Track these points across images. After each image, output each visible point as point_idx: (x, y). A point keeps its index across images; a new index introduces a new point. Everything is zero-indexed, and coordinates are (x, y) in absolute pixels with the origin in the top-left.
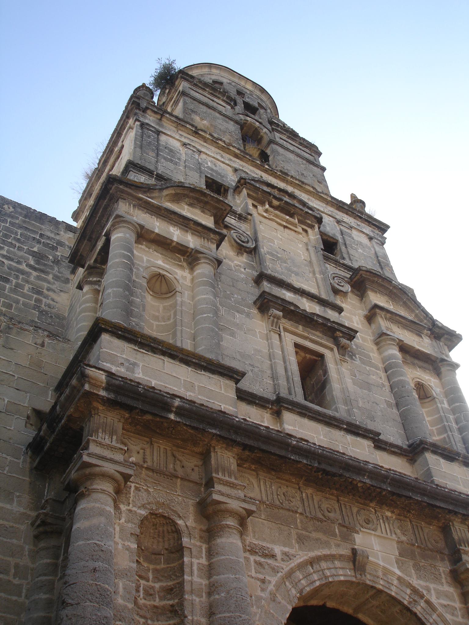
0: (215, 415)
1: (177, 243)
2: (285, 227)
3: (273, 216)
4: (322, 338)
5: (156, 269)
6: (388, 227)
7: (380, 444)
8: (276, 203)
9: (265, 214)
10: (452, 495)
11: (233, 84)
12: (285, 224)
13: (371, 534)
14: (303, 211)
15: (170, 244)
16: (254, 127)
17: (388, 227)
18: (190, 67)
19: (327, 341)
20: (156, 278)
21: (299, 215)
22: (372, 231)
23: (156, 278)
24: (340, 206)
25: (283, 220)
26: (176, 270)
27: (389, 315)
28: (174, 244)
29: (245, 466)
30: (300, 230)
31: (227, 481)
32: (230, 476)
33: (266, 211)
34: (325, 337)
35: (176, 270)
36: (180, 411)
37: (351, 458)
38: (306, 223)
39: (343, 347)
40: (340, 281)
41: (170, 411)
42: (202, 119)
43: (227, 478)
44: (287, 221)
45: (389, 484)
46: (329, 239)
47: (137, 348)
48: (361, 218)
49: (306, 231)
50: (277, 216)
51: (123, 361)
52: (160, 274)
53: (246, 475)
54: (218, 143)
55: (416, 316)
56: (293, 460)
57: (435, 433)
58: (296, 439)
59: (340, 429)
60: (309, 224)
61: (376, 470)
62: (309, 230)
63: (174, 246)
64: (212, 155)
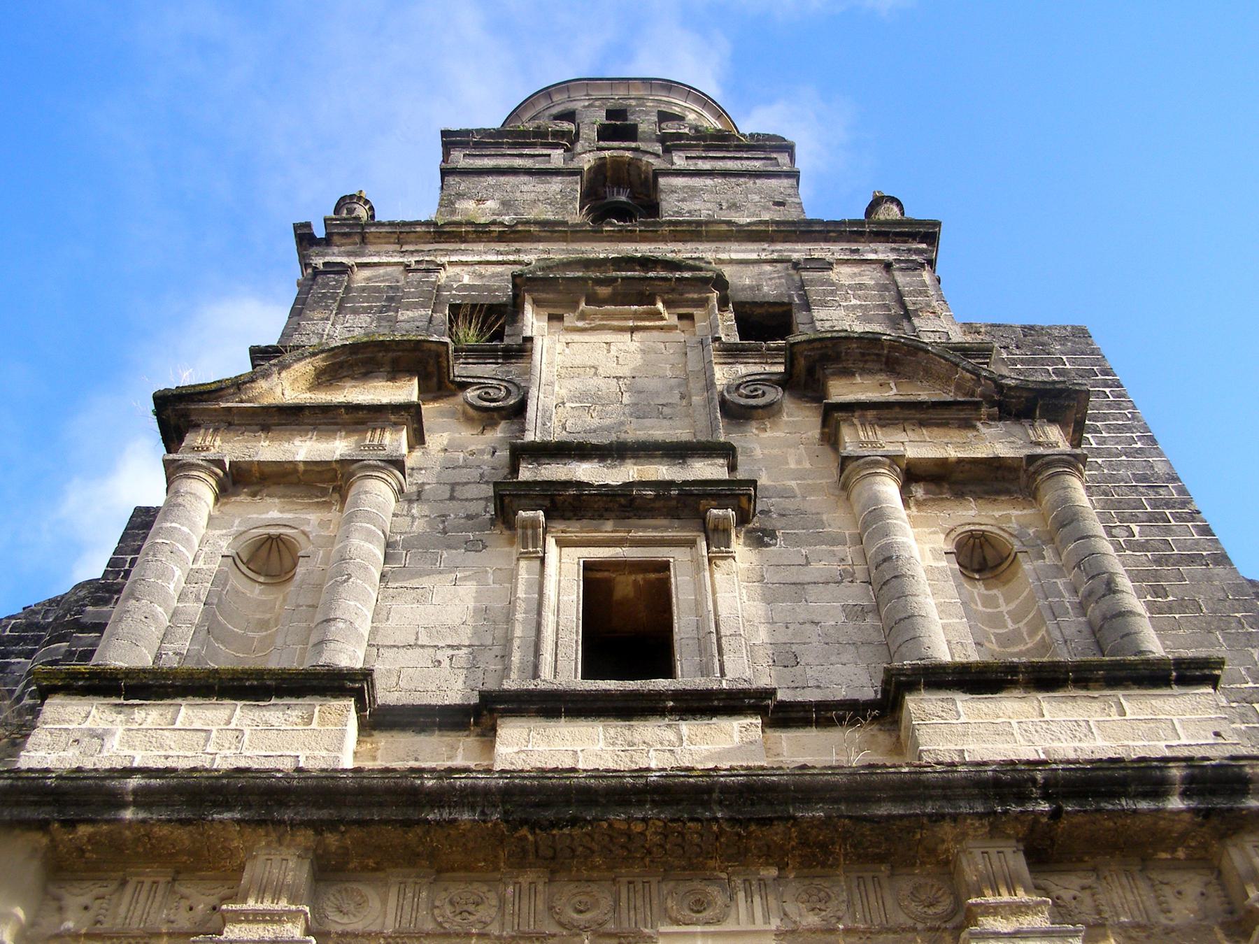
0: (225, 781)
1: (305, 462)
2: (633, 330)
3: (602, 319)
4: (666, 529)
5: (262, 531)
6: (937, 224)
7: (783, 715)
8: (604, 291)
9: (580, 324)
10: (923, 777)
11: (597, 103)
12: (631, 323)
13: (694, 934)
14: (670, 279)
15: (296, 471)
16: (624, 163)
17: (937, 224)
18: (515, 114)
19: (682, 528)
20: (268, 545)
21: (662, 293)
22: (893, 250)
23: (268, 545)
24: (802, 232)
25: (626, 319)
26: (308, 517)
27: (871, 414)
28: (301, 467)
29: (351, 866)
30: (674, 320)
31: (1008, 904)
32: (1011, 890)
33: (582, 317)
34: (676, 523)
35: (308, 517)
36: (144, 798)
37: (596, 774)
38: (687, 300)
39: (716, 529)
40: (752, 388)
41: (125, 805)
42: (480, 201)
43: (1006, 898)
44: (636, 316)
45: (720, 803)
46: (771, 310)
47: (122, 701)
48: (861, 234)
49: (690, 317)
50: (610, 316)
51: (77, 735)
52: (270, 538)
53: (354, 886)
54: (490, 232)
55: (959, 387)
56: (438, 823)
57: (1025, 635)
58: (436, 775)
59: (661, 712)
60: (693, 300)
61: (669, 781)
62: (698, 313)
63: (305, 471)
64: (477, 258)
